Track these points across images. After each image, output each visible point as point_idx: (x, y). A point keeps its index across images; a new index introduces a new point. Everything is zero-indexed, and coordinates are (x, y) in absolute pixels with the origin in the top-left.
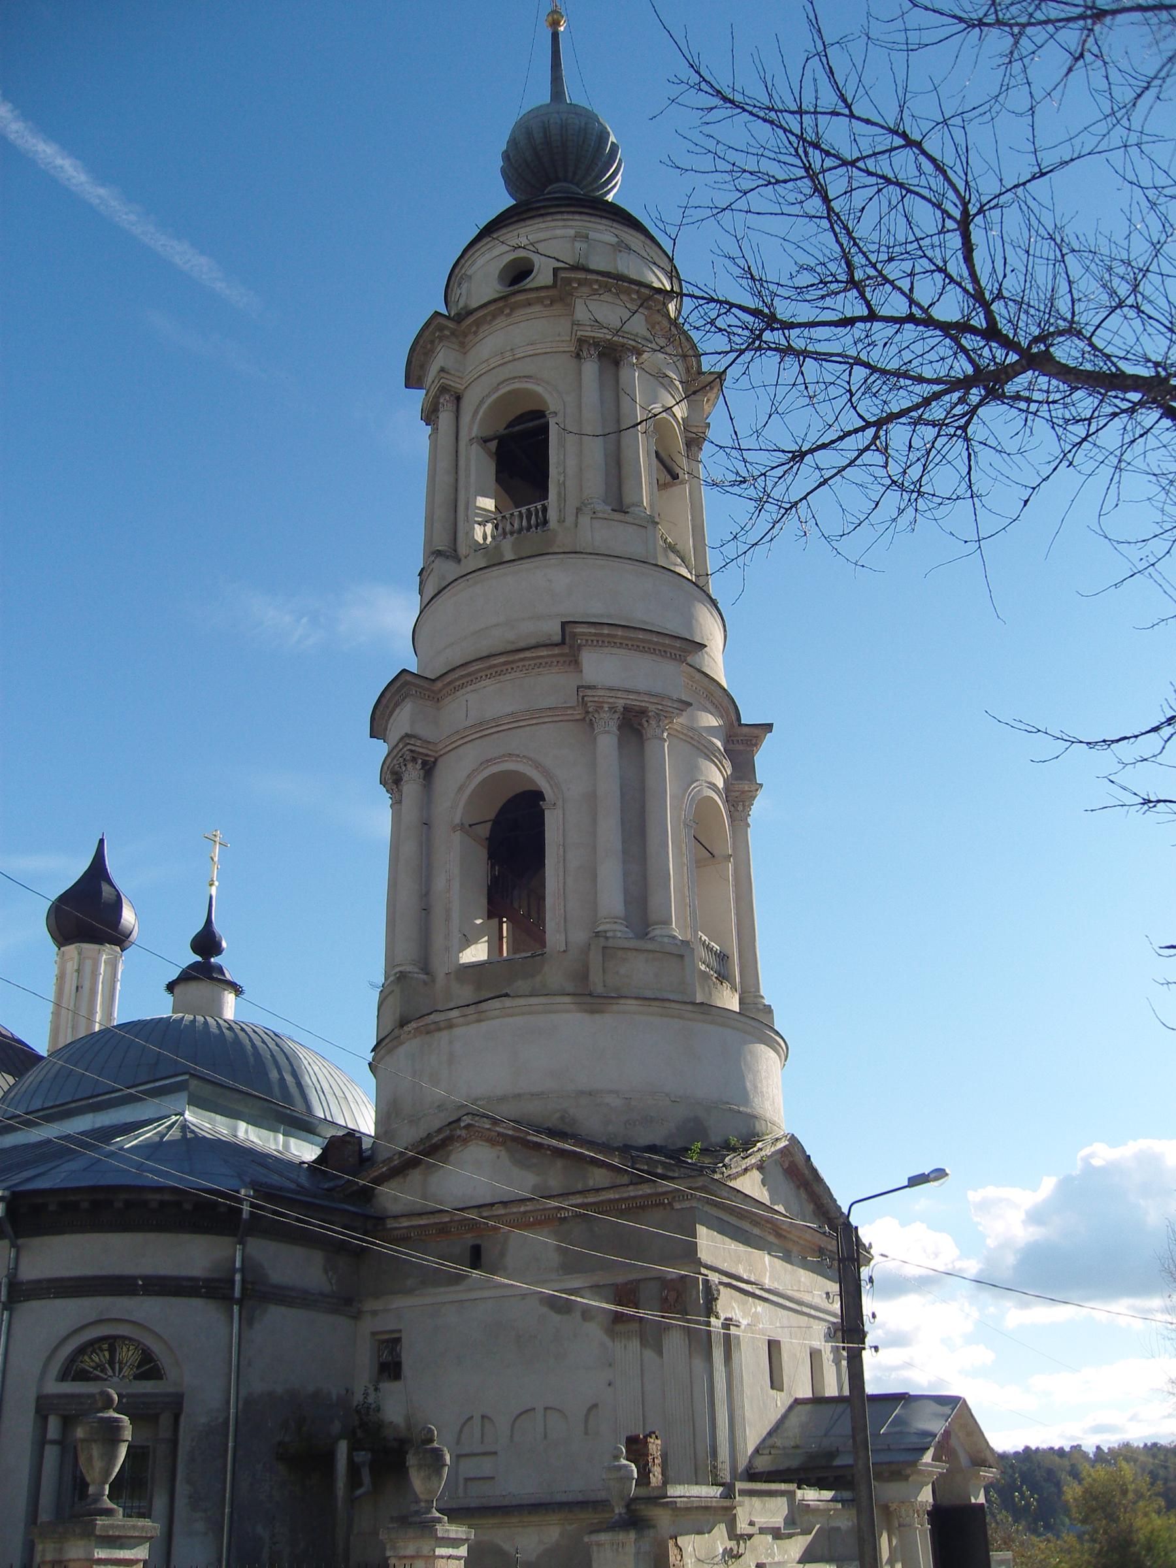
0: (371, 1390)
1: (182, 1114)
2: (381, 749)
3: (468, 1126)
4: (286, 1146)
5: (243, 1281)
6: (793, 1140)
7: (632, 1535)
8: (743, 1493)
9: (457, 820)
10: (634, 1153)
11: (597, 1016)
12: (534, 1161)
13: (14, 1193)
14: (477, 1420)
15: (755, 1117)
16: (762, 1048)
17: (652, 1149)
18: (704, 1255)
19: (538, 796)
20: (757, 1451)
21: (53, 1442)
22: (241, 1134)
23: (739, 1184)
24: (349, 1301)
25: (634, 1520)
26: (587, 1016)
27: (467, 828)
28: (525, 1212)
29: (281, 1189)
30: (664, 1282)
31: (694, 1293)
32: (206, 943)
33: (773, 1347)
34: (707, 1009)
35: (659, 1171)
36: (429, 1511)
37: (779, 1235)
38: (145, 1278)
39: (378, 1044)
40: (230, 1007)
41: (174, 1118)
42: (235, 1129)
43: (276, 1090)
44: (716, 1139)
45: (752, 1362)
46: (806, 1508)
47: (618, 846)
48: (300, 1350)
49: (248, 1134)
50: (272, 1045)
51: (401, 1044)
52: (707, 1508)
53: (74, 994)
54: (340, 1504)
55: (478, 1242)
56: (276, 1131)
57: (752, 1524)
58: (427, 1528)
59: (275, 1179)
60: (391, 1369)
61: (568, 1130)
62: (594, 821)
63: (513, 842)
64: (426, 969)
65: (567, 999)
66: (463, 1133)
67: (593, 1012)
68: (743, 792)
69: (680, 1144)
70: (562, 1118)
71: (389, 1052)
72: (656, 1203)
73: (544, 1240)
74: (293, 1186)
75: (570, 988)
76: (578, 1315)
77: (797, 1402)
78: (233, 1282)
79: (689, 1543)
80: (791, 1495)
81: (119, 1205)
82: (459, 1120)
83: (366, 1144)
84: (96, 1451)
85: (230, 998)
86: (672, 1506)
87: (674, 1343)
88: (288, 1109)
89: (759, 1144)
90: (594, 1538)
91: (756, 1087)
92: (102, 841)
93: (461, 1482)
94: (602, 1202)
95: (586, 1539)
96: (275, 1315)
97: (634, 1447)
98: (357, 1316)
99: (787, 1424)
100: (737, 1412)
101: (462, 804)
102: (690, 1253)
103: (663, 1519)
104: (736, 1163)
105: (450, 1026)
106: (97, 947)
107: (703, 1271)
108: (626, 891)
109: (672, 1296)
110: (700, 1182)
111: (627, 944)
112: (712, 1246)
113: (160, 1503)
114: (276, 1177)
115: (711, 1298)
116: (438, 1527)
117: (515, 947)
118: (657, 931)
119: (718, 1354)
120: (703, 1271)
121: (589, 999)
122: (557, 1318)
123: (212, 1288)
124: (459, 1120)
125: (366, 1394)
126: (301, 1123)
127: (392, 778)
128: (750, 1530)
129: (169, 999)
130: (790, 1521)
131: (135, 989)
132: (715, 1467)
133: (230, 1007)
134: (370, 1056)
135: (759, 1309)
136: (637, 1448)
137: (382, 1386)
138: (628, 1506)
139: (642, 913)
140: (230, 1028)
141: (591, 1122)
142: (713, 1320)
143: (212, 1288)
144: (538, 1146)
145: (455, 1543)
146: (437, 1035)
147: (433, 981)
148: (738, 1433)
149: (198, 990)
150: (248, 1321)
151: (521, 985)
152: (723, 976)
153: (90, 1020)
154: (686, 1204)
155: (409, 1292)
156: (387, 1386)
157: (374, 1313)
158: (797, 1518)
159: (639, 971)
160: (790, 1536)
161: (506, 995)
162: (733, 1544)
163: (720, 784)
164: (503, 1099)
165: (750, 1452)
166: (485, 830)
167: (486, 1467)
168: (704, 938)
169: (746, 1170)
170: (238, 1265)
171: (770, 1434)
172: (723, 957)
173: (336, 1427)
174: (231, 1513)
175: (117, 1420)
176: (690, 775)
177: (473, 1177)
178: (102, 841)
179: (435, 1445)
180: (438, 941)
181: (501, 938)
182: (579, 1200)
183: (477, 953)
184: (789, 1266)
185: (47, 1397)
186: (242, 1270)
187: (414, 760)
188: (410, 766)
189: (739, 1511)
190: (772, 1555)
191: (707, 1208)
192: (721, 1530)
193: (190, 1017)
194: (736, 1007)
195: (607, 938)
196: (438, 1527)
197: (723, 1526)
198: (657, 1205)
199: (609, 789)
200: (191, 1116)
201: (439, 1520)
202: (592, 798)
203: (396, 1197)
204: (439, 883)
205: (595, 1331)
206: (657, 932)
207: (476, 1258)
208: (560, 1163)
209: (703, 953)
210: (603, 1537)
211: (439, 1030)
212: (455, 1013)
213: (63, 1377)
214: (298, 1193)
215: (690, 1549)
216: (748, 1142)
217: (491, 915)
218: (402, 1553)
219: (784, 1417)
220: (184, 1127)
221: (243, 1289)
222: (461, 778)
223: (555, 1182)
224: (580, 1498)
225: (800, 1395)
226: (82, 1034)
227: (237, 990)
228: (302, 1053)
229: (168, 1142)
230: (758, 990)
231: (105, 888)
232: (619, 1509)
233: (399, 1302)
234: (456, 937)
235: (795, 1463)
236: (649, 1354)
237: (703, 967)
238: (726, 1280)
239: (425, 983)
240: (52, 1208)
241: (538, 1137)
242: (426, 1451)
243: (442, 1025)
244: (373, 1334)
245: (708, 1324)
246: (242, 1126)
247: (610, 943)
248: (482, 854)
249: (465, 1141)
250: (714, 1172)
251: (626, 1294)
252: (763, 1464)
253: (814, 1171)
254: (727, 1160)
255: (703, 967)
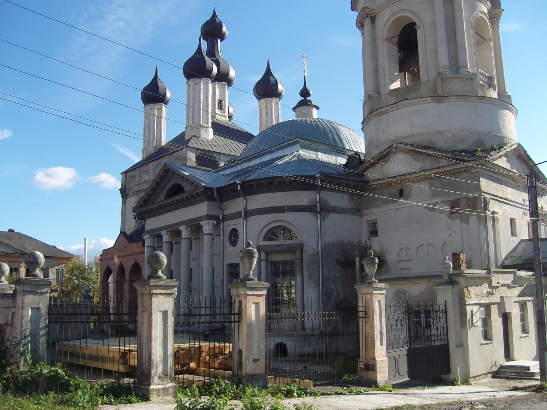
0: (368, 240)
1: (298, 151)
2: (356, 14)
3: (396, 147)
4: (336, 160)
5: (320, 206)
6: (519, 145)
7: (450, 287)
8: (494, 272)
9: (385, 37)
10: (456, 153)
11: (441, 104)
12: (420, 158)
13: (242, 182)
14: (404, 250)
15: (503, 137)
16: (506, 111)
17: (463, 151)
18: (483, 188)
19: (414, 24)
20: (506, 258)
21: (264, 260)
22: (320, 157)
23: (498, 162)
24: (358, 211)
25: (452, 281)
26: (437, 104)
27: (389, 40)
28: (417, 177)
29: (330, 174)
30: (468, 199)
31: (480, 202)
32: (305, 93)
33: (512, 221)
34: (484, 99)
35: (465, 159)
36: (371, 278)
37: (514, 181)
38: (287, 206)
39: (364, 120)
40: (315, 114)
41: (296, 153)
42: (317, 155)
43: (332, 141)
44: (488, 146)
45: (503, 227)
46: (520, 278)
47: (446, 39)
48: (342, 228)
49: (322, 157)
50: (329, 126)
51: (371, 120)
52: (479, 277)
53: (265, 114)
54: (358, 277)
55: (402, 188)
56: (332, 155)
57: (498, 283)
58: (370, 284)
59: (330, 171)
60: (374, 233)
61: (432, 146)
62: (436, 31)
63: (407, 42)
64: (378, 93)
65: (429, 99)
66: (394, 150)
67: (439, 102)
68: (496, 14)
69: (474, 149)
70: (430, 142)
71: (367, 123)
72: (465, 170)
73: (424, 187)
74: (336, 173)
75: (430, 94)
76: (438, 211)
77: (522, 241)
78: (317, 206)
79: (472, 289)
80: (514, 273)
81: (276, 183)
82: (392, 145)
83: (362, 157)
84: (246, 260)
85: (314, 111)
86: (465, 277)
87: (473, 220)
88: (337, 148)
89: (505, 147)
90: (437, 287)
91: (504, 126)
92: (268, 62)
93: (400, 269)
94: (445, 171)
95: (434, 288)
96: (332, 216)
97: (455, 257)
98: (362, 216)
99: (518, 248)
100: (498, 244)
101: (386, 31)
102: (478, 188)
103: (462, 281)
104: (495, 154)
105: (387, 112)
106: (270, 99)
107: (483, 194)
108: (449, 56)
109: (472, 204)
110: (481, 162)
111: (450, 76)
112: (486, 185)
113: (299, 278)
114: (330, 170)
115: (486, 204)
116: (374, 284)
117: (412, 81)
118: (462, 70)
119: (490, 224)
120: (483, 194)
121: (437, 98)
122: (431, 213)
123: (310, 209)
124: (392, 145)
125: (366, 242)
126: (339, 150)
127: (360, 25)
128: (498, 285)
129: (294, 113)
130: (514, 282)
131: (284, 111)
132: (489, 264)
133: (315, 114)
134: (361, 126)
135: (506, 208)
136: (456, 257)
137: (371, 238)
138: (449, 277)
139: (456, 64)
140: (315, 121)
141: (441, 143)
142: (487, 212)
143: (310, 209)
144: (421, 153)
145: (381, 289)
146: (383, 116)
147: (381, 97)
148: (498, 251)
149: (303, 109)
150: (323, 218)
151: (412, 95)
152: (491, 85)
153: (272, 121)
154: (476, 170)
155: (379, 206)
156: (373, 239)
157: (367, 214)
158: (517, 282)
159: (456, 86)
160: (514, 287)
161: (407, 99)
162: (490, 290)
163: (486, 11)
164: (407, 137)
165: (503, 259)
166: (396, 40)
167: (408, 265)
168: (482, 71)
169: (500, 157)
170: (318, 200)
171: (511, 252)
172: (490, 78)
173: (357, 253)
174: (322, 281)
175: (252, 250)
176: (473, 8)
177: (399, 165)
178: (268, 62)
179: (372, 256)
180: (382, 82)
181: (405, 79)
182: (436, 171)
183: (396, 85)
184: (519, 192)
185: (260, 246)
186: (320, 202)
187: (367, 17)
188: (366, 19)
189: (493, 278)
190: (507, 294)
191: (484, 171)
192: (485, 285)
193: (300, 119)
194: (496, 97)
195: (443, 75)
196: (374, 284)
197: (486, 284)
198: (465, 171)
199: (440, 18)
200: (302, 152)
201: (375, 282)
202: (434, 22)
203: (372, 174)
204: (381, 61)
205: (444, 217)
206: (462, 71)
207: (401, 194)
208: (429, 158)
209: (481, 77)
210: (440, 287)
211: (384, 114)
212: (388, 107)
213: (265, 239)
214: (337, 175)
215: (473, 291)
216: (501, 146)
217: (401, 71)
218: (362, 293)
219: (517, 246)
220: (299, 156)
221: (320, 208)
222: (385, 20)
223: (428, 165)
224: (433, 274)
225: (524, 238)
226: (269, 126)
227: (317, 108)
228: (340, 127)
229: (294, 161)
230: (505, 90)
231: (271, 78)
232: (446, 278)
233: (375, 210)
234: (388, 80)
235: (520, 262)
236: (464, 224)
237: (482, 83)
238: (492, 197)
239: (378, 98)
240: (255, 186)
241: (419, 149)
242: (369, 259)
243: (384, 112)
244: (368, 221)
245: (485, 213)
246: (320, 154)
247: (444, 76)
248: (396, 49)
249: (395, 153)
250: (486, 158)
251: (455, 204)
252: (508, 263)
253: (528, 156)
254: (491, 153)
255: (482, 83)
